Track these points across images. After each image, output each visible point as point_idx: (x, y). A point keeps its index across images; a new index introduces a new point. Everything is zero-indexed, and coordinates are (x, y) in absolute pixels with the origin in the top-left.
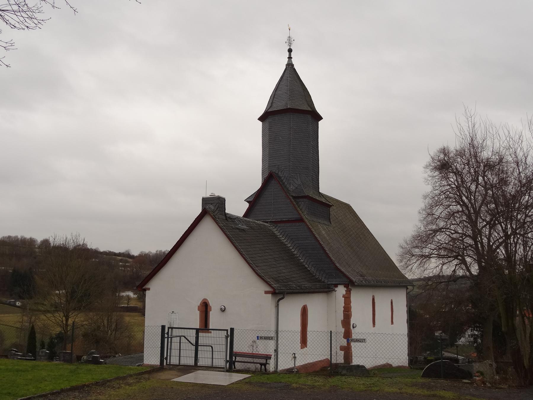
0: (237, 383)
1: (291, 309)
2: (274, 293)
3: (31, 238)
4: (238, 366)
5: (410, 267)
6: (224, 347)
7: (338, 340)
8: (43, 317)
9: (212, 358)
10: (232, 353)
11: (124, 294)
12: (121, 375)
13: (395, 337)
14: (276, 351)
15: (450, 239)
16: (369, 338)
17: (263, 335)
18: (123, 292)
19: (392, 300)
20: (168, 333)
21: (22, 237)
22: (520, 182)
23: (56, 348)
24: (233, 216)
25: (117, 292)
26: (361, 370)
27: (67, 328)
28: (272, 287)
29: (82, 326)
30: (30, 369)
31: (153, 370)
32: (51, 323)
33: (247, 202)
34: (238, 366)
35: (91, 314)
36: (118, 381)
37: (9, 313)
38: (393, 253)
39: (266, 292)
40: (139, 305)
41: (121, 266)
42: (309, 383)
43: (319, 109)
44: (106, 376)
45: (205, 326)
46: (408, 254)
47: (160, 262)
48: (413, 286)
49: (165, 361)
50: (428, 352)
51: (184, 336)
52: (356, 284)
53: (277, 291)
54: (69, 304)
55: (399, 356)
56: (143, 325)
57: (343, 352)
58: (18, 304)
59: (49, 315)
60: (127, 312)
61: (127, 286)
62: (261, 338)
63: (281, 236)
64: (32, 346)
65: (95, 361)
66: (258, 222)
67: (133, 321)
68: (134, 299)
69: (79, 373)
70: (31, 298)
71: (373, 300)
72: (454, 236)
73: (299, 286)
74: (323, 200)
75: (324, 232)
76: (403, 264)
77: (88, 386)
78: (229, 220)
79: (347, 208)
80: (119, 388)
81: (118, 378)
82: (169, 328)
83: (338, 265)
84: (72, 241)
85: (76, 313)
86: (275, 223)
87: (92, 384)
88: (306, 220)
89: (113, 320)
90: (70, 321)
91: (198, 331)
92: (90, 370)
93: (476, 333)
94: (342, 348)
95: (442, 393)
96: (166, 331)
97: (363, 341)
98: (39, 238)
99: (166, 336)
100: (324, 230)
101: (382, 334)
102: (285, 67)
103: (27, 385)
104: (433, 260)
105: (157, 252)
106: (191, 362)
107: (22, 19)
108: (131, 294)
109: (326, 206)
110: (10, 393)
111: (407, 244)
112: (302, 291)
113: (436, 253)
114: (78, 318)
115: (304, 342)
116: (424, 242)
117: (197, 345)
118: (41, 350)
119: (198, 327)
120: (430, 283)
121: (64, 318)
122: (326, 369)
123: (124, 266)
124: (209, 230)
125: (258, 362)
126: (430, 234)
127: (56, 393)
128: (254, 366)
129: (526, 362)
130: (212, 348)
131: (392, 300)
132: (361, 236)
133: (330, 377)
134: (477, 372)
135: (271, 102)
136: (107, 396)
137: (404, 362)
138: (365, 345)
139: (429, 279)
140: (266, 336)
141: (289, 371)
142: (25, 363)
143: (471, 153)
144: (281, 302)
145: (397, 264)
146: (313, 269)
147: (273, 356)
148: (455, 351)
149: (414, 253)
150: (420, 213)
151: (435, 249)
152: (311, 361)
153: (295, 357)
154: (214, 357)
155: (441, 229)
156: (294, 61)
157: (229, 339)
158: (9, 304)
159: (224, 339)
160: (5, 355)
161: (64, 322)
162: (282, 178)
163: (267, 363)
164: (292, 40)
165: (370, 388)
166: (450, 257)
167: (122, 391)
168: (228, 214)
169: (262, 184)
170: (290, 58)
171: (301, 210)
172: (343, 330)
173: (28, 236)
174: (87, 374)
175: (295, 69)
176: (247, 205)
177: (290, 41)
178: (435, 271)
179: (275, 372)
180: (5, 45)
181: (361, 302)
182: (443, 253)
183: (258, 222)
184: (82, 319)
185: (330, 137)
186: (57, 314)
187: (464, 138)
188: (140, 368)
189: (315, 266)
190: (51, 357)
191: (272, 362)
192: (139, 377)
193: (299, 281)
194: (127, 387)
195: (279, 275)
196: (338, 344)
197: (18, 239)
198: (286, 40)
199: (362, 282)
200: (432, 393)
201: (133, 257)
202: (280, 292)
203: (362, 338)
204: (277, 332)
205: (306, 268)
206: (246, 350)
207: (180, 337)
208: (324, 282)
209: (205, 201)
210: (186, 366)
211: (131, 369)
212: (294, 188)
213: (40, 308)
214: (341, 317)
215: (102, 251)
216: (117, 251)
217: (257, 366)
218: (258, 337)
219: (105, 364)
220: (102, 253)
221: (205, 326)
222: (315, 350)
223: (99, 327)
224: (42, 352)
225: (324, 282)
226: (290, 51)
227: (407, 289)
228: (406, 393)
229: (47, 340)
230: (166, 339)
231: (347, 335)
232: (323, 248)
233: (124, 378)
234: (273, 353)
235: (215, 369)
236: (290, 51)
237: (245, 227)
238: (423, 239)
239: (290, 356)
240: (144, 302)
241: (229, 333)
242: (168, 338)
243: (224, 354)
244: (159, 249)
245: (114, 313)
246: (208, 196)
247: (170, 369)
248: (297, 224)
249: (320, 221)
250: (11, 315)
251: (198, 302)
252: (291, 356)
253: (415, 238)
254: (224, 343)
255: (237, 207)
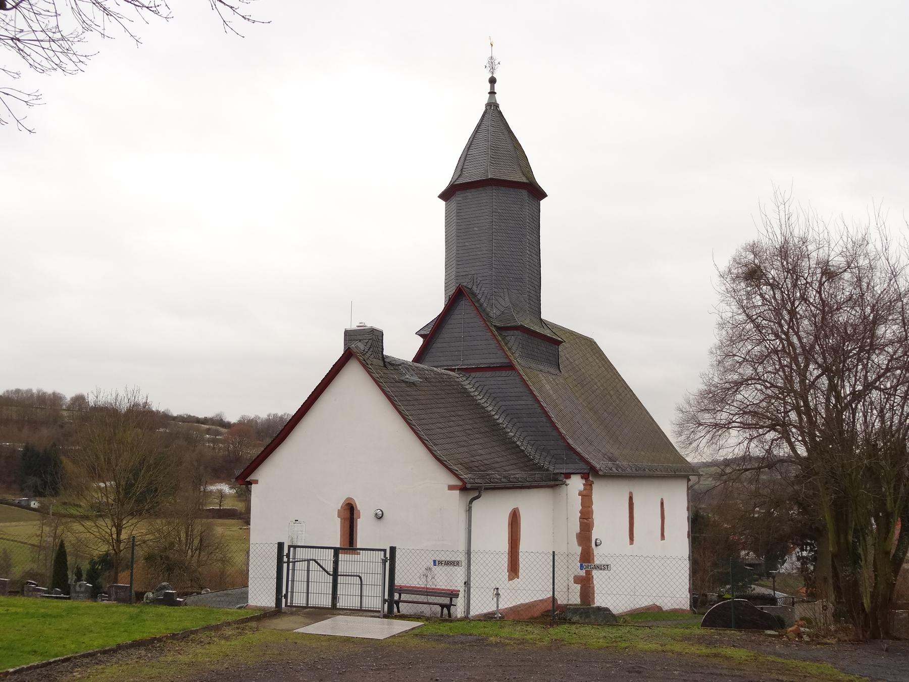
0: (400, 635)
1: (492, 513)
2: (464, 489)
3: (54, 394)
4: (404, 608)
5: (694, 444)
6: (380, 577)
7: (570, 567)
8: (76, 526)
9: (361, 596)
10: (392, 588)
11: (213, 488)
12: (213, 623)
13: (668, 562)
14: (467, 584)
15: (762, 397)
16: (615, 563)
17: (443, 559)
18: (212, 484)
19: (662, 499)
20: (288, 555)
21: (39, 391)
22: (816, 326)
23: (101, 578)
24: (395, 359)
25: (200, 485)
26: (605, 617)
27: (119, 546)
28: (461, 480)
29: (144, 542)
30: (64, 614)
31: (265, 615)
32: (91, 538)
33: (421, 336)
34: (404, 608)
35: (159, 521)
36: (208, 633)
37: (19, 520)
38: (667, 421)
39: (451, 488)
40: (239, 506)
41: (209, 441)
42: (517, 635)
43: (541, 179)
44: (188, 625)
45: (349, 543)
46: (691, 421)
47: (277, 434)
48: (699, 476)
49: (284, 600)
50: (728, 586)
51: (315, 560)
52: (600, 473)
53: (469, 486)
54: (123, 505)
55: (675, 593)
56: (247, 540)
57: (578, 587)
58: (34, 504)
59: (89, 524)
60: (220, 517)
61: (219, 474)
62: (440, 563)
63: (476, 393)
64: (61, 575)
65: (169, 601)
66: (439, 370)
67: (229, 533)
68: (230, 496)
69: (144, 621)
70: (56, 493)
71: (631, 499)
72: (769, 392)
73: (505, 478)
74: (548, 333)
75: (548, 387)
76: (683, 438)
77: (160, 640)
78: (389, 367)
79: (590, 345)
80: (209, 643)
81: (208, 628)
82: (290, 547)
83: (570, 441)
84: (126, 401)
85: (134, 521)
86: (467, 371)
87: (167, 636)
88: (518, 367)
89: (195, 532)
90: (124, 536)
91: (337, 551)
92: (162, 615)
93: (805, 554)
94: (577, 580)
95: (729, 651)
96: (286, 551)
97: (606, 567)
98: (68, 393)
99: (285, 559)
100: (549, 382)
101: (645, 557)
102: (484, 109)
103: (61, 638)
104: (734, 432)
105: (269, 416)
106: (327, 602)
107: (51, 54)
108: (225, 488)
109: (550, 343)
110: (35, 652)
111: (690, 405)
112: (510, 485)
113: (738, 420)
114: (137, 529)
115: (514, 569)
116: (718, 402)
117: (335, 574)
118: (79, 583)
119: (338, 546)
120: (728, 470)
121: (114, 529)
122: (551, 614)
123: (214, 441)
124: (356, 384)
125: (436, 601)
126: (729, 389)
127: (109, 650)
128: (428, 609)
129: (867, 602)
130: (360, 578)
131: (662, 499)
132: (612, 392)
133: (551, 625)
134: (802, 619)
135: (460, 168)
136: (190, 656)
137: (683, 602)
138: (609, 574)
139: (727, 463)
140: (448, 559)
141: (489, 617)
142: (55, 603)
143: (789, 255)
144: (475, 502)
145: (673, 439)
146: (529, 448)
147: (461, 595)
148: (770, 584)
149: (702, 421)
150: (712, 353)
151: (736, 414)
152: (527, 601)
153: (498, 595)
154: (364, 594)
155: (747, 380)
156: (499, 98)
157: (388, 564)
158: (19, 505)
159: (380, 565)
160: (19, 589)
161: (115, 536)
162: (479, 297)
163: (451, 605)
164: (496, 62)
165: (614, 644)
166: (762, 427)
167: (214, 649)
168: (387, 357)
169: (446, 305)
170: (492, 93)
171: (510, 349)
172: (579, 550)
173: (49, 389)
174: (157, 621)
175: (500, 113)
176: (420, 341)
177: (492, 65)
178: (736, 451)
179: (466, 618)
180: (26, 98)
181: (609, 503)
182: (749, 419)
183: (439, 370)
184: (144, 531)
185: (558, 226)
186: (101, 522)
187: (771, 236)
188: (243, 611)
189: (532, 442)
190: (95, 594)
191: (460, 602)
192: (242, 625)
193: (507, 468)
194: (223, 642)
195: (472, 459)
196: (570, 573)
197: (32, 395)
198: (486, 62)
199: (611, 469)
200: (714, 651)
201: (227, 425)
202: (473, 486)
203: (604, 563)
204: (469, 553)
205: (518, 446)
206: (416, 583)
207: (308, 561)
208: (547, 470)
209: (350, 336)
210: (318, 608)
211: (227, 613)
212: (498, 313)
213: (73, 511)
214: (577, 528)
215: (175, 415)
216: (201, 415)
217: (433, 609)
218: (434, 561)
219: (186, 604)
220: (174, 418)
221: (349, 543)
222: (532, 583)
223: (172, 544)
224: (80, 586)
225: (547, 470)
226: (493, 81)
227: (689, 480)
228: (672, 652)
229: (85, 566)
230: (285, 565)
231: (586, 557)
232: (546, 413)
233: (217, 628)
234: (461, 588)
235: (365, 614)
236: (493, 81)
237: (415, 379)
238: (716, 397)
239: (490, 591)
240: (248, 502)
241: (388, 556)
242: (288, 562)
243: (380, 588)
244: (273, 412)
245: (198, 521)
246: (354, 326)
247: (292, 614)
248: (504, 373)
249: (542, 367)
250: (22, 523)
251: (338, 504)
252: (492, 592)
253: (703, 395)
254: (380, 570)
255: (402, 346)
